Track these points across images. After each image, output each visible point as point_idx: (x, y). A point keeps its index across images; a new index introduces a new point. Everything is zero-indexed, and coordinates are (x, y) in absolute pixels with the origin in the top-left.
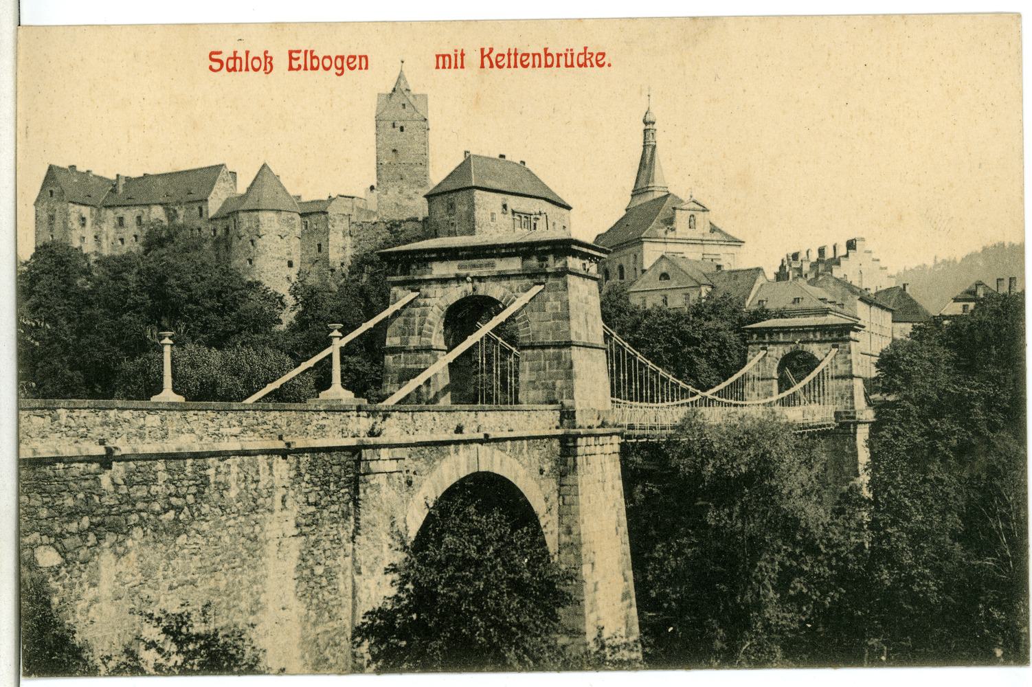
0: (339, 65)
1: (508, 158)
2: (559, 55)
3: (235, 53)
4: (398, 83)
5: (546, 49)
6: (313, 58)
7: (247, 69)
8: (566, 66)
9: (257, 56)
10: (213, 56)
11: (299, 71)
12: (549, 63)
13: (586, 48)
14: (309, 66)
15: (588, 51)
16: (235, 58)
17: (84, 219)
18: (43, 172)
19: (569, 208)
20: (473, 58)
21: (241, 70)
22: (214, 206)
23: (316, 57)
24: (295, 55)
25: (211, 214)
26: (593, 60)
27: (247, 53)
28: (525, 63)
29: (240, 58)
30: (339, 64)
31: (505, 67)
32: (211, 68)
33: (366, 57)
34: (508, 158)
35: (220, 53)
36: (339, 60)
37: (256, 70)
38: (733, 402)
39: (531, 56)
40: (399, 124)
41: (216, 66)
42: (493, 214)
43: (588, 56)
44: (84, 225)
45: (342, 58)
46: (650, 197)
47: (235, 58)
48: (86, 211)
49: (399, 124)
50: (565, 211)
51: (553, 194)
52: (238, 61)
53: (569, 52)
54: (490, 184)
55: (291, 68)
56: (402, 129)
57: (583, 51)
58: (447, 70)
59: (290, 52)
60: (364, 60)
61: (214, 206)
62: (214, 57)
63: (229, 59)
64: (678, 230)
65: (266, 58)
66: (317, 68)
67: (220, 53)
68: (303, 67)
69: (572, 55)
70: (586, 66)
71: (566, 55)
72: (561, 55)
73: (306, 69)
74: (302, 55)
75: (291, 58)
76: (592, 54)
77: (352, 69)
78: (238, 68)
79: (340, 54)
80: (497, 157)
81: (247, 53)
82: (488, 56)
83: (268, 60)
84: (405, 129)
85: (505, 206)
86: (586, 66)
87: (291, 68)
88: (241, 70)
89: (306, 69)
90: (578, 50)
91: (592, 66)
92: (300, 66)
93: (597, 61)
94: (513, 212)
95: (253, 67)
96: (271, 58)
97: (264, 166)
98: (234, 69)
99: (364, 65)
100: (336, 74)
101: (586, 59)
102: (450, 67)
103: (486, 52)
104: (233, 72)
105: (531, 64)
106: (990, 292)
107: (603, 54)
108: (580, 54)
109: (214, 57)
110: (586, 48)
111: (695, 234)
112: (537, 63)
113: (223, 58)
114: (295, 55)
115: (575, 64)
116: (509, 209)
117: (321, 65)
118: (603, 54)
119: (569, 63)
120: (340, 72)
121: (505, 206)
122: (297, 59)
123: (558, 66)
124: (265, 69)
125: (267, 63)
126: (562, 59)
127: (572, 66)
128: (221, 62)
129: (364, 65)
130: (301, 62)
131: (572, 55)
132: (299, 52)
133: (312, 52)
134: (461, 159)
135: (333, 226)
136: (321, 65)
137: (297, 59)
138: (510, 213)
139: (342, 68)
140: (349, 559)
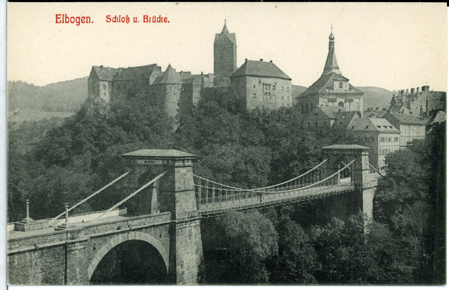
0: (78, 21)
1: (264, 61)
3: (115, 16)
4: (224, 29)
5: (127, 16)
6: (66, 18)
7: (120, 22)
8: (153, 22)
10: (108, 17)
11: (147, 23)
12: (67, 21)
13: (160, 16)
15: (161, 17)
16: (115, 18)
17: (105, 86)
18: (92, 67)
19: (291, 80)
20: (140, 19)
22: (152, 81)
23: (68, 17)
24: (58, 16)
25: (151, 84)
26: (163, 20)
27: (120, 16)
28: (83, 21)
29: (117, 18)
30: (78, 20)
31: (167, 22)
32: (107, 21)
33: (89, 17)
34: (264, 61)
35: (110, 16)
36: (78, 19)
37: (123, 22)
38: (228, 186)
39: (86, 18)
41: (109, 20)
42: (254, 86)
43: (161, 19)
44: (105, 88)
45: (79, 18)
47: (115, 18)
48: (106, 83)
50: (289, 81)
51: (288, 76)
53: (154, 17)
54: (254, 73)
55: (57, 22)
57: (114, 17)
58: (88, 23)
59: (57, 15)
60: (88, 19)
61: (152, 81)
62: (108, 17)
63: (113, 18)
64: (335, 89)
65: (127, 18)
67: (110, 16)
68: (62, 22)
69: (155, 18)
70: (160, 22)
73: (63, 22)
74: (61, 16)
75: (57, 18)
76: (162, 18)
77: (83, 23)
79: (79, 16)
80: (259, 60)
81: (120, 16)
83: (128, 18)
85: (260, 82)
86: (160, 22)
87: (57, 22)
89: (63, 22)
90: (157, 16)
92: (61, 21)
93: (164, 20)
94: (264, 84)
96: (129, 18)
97: (170, 65)
98: (115, 21)
99: (135, 19)
100: (77, 25)
101: (160, 19)
102: (118, 22)
106: (65, 167)
107: (166, 18)
108: (158, 18)
109: (108, 17)
110: (160, 16)
111: (342, 90)
113: (111, 17)
114: (58, 16)
115: (156, 21)
116: (262, 83)
118: (166, 18)
119: (154, 21)
120: (78, 24)
121: (260, 82)
122: (59, 18)
123: (150, 22)
124: (127, 21)
126: (152, 19)
127: (155, 22)
129: (135, 19)
130: (61, 19)
131: (155, 18)
132: (60, 15)
133: (66, 15)
134: (244, 62)
135: (194, 89)
137: (59, 18)
138: (262, 85)
139: (79, 22)
140: (63, 277)
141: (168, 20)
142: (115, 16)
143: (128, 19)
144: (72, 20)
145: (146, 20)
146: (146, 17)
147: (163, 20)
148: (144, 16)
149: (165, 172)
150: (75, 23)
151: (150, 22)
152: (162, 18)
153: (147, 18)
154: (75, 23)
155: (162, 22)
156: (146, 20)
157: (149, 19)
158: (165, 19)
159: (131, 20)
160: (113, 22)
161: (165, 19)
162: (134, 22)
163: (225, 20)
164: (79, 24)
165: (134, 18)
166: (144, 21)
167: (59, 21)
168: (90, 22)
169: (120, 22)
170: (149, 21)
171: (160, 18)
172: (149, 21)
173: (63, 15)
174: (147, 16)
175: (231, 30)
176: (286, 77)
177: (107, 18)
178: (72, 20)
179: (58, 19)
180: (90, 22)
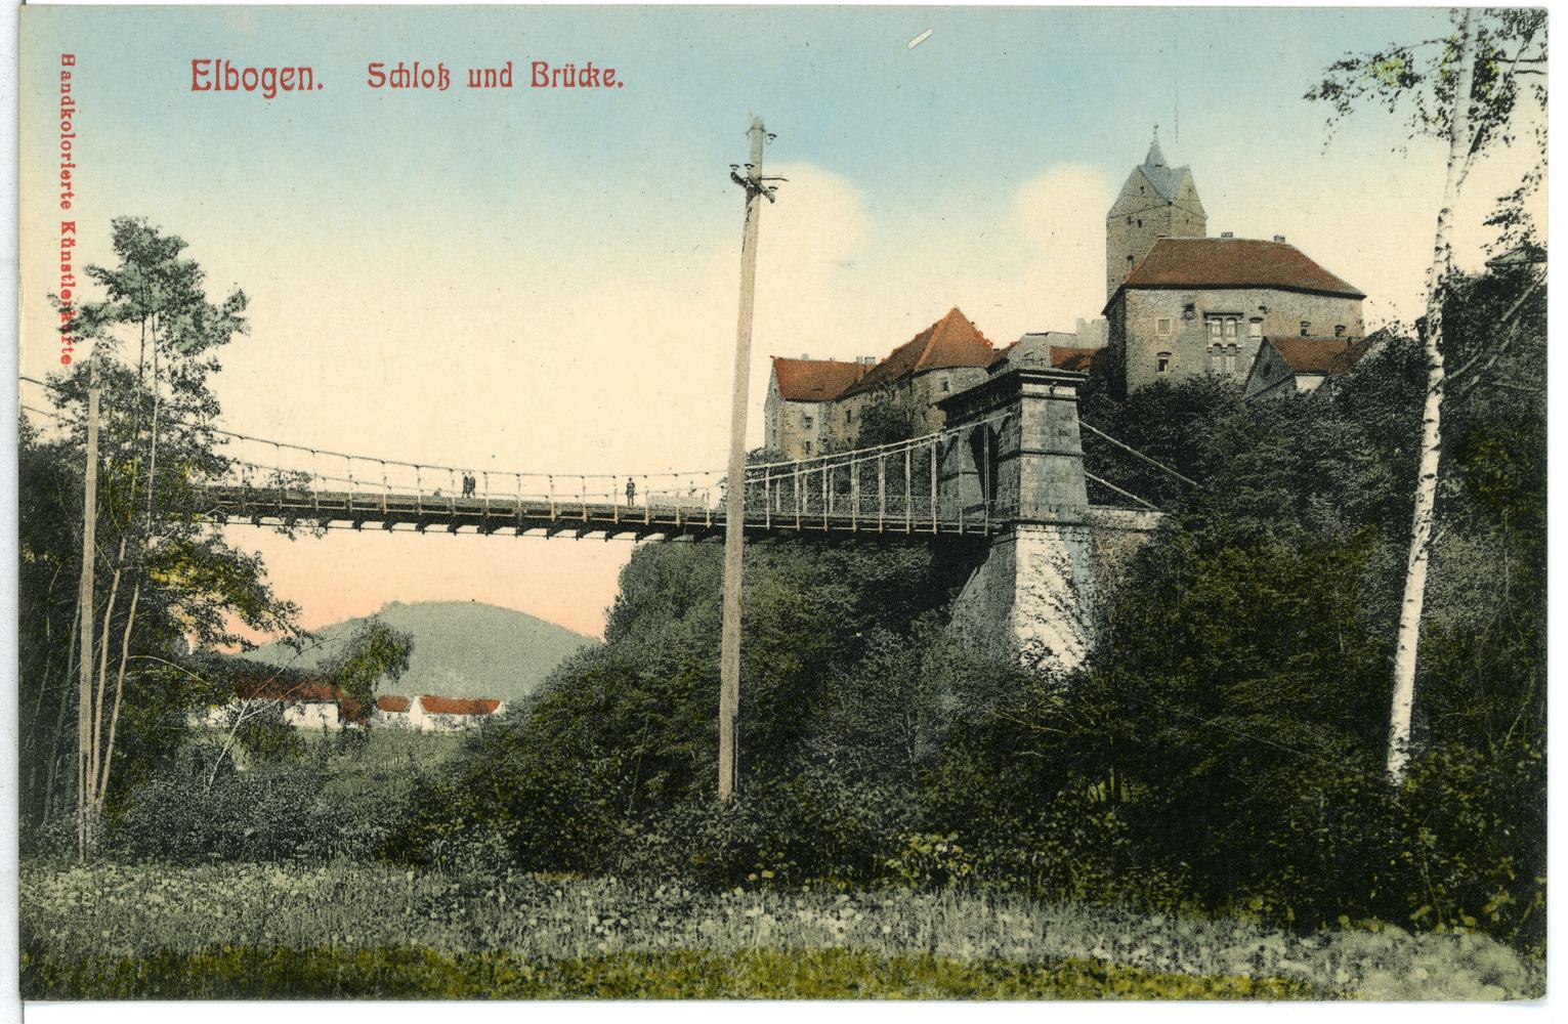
0: (269, 83)
2: (556, 72)
3: (401, 65)
6: (228, 71)
7: (416, 85)
8: (566, 85)
9: (251, 67)
10: (374, 69)
12: (232, 83)
13: (589, 64)
14: (222, 84)
15: (593, 67)
19: (1360, 297)
20: (521, 74)
21: (408, 85)
24: (201, 67)
26: (600, 77)
27: (416, 64)
29: (407, 72)
32: (370, 82)
33: (310, 70)
35: (381, 65)
36: (269, 75)
39: (297, 73)
40: (1135, 217)
41: (377, 80)
43: (593, 74)
45: (273, 71)
46: (1004, 370)
49: (1135, 217)
52: (405, 74)
53: (569, 69)
55: (195, 87)
56: (1140, 222)
58: (491, 89)
59: (195, 63)
60: (306, 74)
62: (374, 69)
65: (441, 70)
66: (235, 88)
67: (381, 65)
68: (213, 86)
69: (573, 71)
71: (565, 71)
72: (559, 71)
74: (212, 67)
75: (196, 71)
76: (597, 71)
78: (404, 83)
81: (416, 64)
82: (594, 77)
83: (444, 74)
84: (1144, 222)
85: (1190, 307)
86: (401, 86)
87: (195, 87)
88: (408, 85)
89: (218, 88)
91: (598, 84)
93: (605, 79)
94: (1206, 315)
95: (424, 84)
101: (590, 77)
103: (72, 60)
104: (398, 88)
105: (297, 85)
107: (613, 71)
108: (582, 71)
109: (374, 69)
110: (589, 64)
112: (491, 82)
113: (386, 70)
114: (201, 67)
116: (1198, 311)
117: (241, 83)
118: (613, 71)
119: (569, 82)
120: (269, 93)
121: (1190, 307)
122: (205, 73)
123: (555, 85)
124: (440, 84)
125: (541, 75)
127: (573, 84)
128: (382, 75)
130: (212, 78)
132: (207, 62)
136: (241, 83)
137: (205, 73)
138: (1200, 320)
139: (273, 87)
141: (617, 78)
142: (401, 65)
143: (444, 76)
144: (250, 79)
145: (540, 80)
146: (540, 68)
147: (600, 77)
148: (534, 65)
149: (501, 890)
150: (260, 89)
151: (555, 85)
152: (597, 71)
153: (543, 73)
154: (260, 89)
155: (598, 84)
156: (540, 80)
157: (549, 73)
158: (608, 75)
159: (67, 69)
160: (394, 85)
161: (608, 75)
162: (472, 85)
163: (1426, 42)
164: (274, 95)
165: (471, 72)
166: (534, 84)
167: (204, 85)
168: (310, 87)
169: (416, 85)
170: (551, 82)
171: (589, 71)
172: (551, 82)
173: (218, 62)
174: (546, 66)
175: (1173, 161)
176: (1345, 291)
177: (371, 72)
178: (250, 79)
179: (198, 76)
180: (310, 87)
